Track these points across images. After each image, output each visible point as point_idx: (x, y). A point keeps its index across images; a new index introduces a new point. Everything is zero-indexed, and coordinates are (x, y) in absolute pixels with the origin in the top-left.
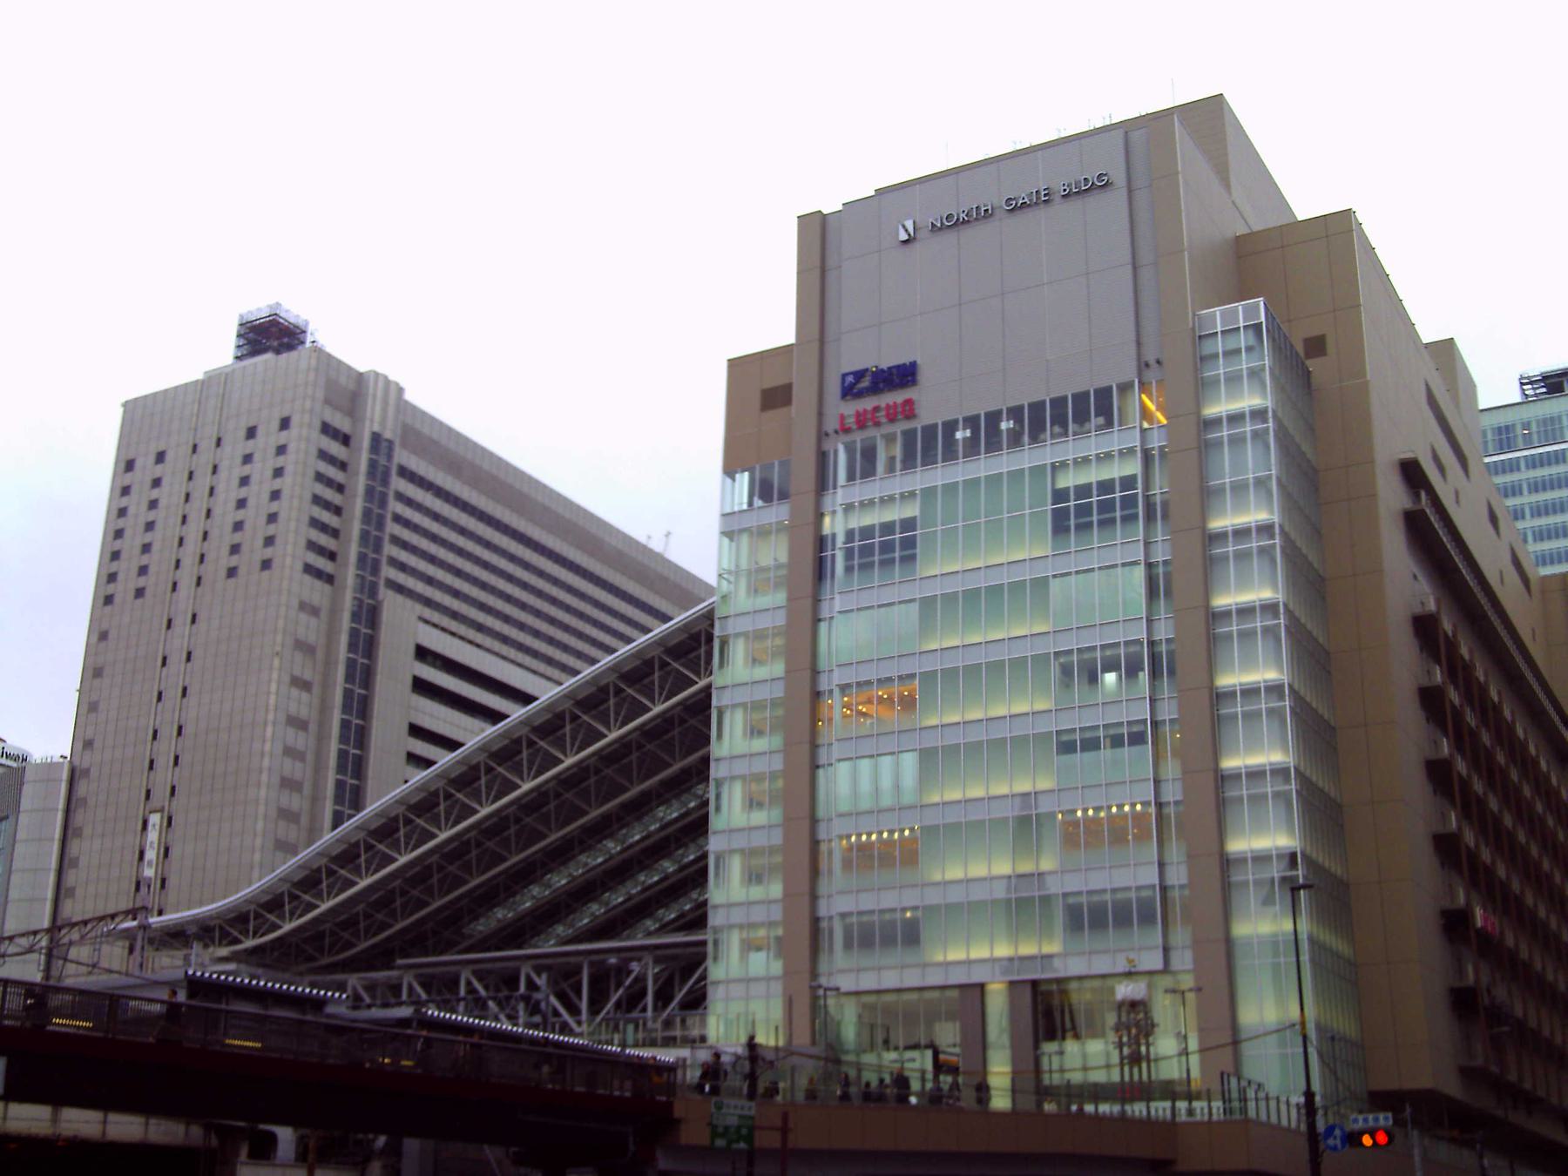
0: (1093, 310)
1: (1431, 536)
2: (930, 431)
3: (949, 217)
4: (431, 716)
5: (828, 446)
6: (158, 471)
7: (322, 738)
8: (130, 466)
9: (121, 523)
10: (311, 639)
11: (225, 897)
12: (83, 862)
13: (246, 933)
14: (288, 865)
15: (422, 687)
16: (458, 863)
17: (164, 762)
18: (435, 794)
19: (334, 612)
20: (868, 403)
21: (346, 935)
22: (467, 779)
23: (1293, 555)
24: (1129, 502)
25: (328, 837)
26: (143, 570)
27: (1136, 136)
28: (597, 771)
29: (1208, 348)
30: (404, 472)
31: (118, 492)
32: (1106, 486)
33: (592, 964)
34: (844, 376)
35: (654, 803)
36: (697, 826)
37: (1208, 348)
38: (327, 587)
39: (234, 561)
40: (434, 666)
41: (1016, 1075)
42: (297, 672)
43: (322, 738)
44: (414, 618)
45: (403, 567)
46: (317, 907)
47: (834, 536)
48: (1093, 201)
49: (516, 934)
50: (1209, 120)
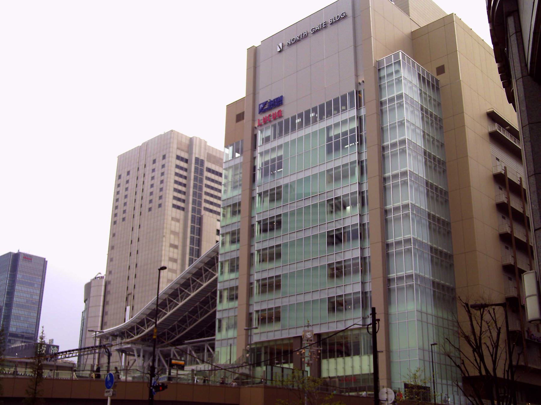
2: (287, 121)
10: (177, 230)
17: (132, 276)
20: (267, 114)
30: (209, 170)
32: (345, 133)
34: (260, 105)
38: (182, 212)
44: (216, 220)
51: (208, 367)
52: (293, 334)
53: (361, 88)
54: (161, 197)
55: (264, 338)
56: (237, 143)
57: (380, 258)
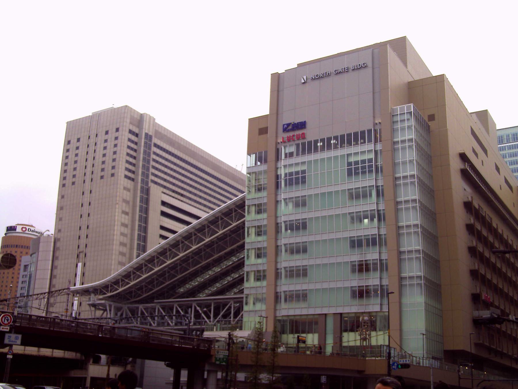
0: (360, 107)
1: (471, 175)
2: (310, 143)
3: (317, 76)
4: (167, 223)
5: (279, 146)
6: (78, 144)
7: (133, 230)
8: (69, 142)
9: (67, 161)
10: (128, 199)
11: (103, 279)
12: (59, 267)
13: (107, 291)
14: (121, 270)
15: (163, 214)
16: (174, 270)
17: (83, 236)
18: (191, 234)
19: (135, 190)
20: (291, 134)
21: (139, 292)
22: (175, 245)
23: (421, 184)
24: (370, 167)
25: (135, 260)
26: (74, 176)
27: (376, 51)
28: (230, 236)
29: (395, 119)
30: (156, 145)
31: (65, 151)
32: (363, 162)
33: (215, 303)
34: (284, 125)
35: (235, 253)
36: (241, 265)
37: (395, 119)
38: (132, 182)
39: (103, 174)
40: (168, 207)
41: (335, 343)
42: (124, 209)
43: (133, 230)
44: (160, 192)
45: (156, 176)
46: (141, 276)
47: (281, 175)
48: (362, 71)
49: (193, 293)
50: (400, 45)
51: (288, 338)
52: (319, 311)
53: (378, 128)
54: (113, 168)
55: (291, 312)
56: (261, 153)
57: (396, 262)
